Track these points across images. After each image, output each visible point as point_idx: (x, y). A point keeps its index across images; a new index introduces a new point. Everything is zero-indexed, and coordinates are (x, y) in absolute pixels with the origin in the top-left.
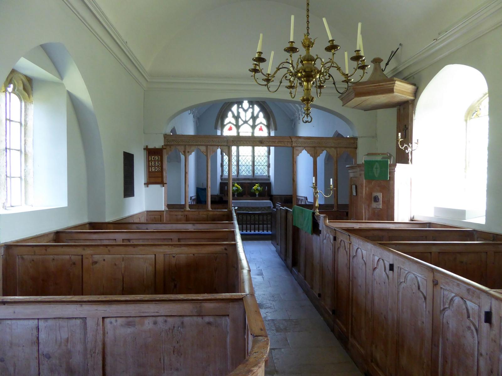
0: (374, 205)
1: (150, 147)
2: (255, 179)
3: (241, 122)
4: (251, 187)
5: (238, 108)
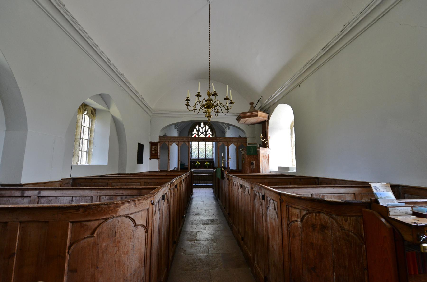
0: (252, 167)
1: (152, 142)
2: (207, 160)
3: (200, 133)
4: (204, 163)
5: (199, 127)
